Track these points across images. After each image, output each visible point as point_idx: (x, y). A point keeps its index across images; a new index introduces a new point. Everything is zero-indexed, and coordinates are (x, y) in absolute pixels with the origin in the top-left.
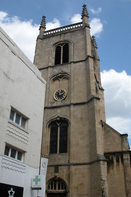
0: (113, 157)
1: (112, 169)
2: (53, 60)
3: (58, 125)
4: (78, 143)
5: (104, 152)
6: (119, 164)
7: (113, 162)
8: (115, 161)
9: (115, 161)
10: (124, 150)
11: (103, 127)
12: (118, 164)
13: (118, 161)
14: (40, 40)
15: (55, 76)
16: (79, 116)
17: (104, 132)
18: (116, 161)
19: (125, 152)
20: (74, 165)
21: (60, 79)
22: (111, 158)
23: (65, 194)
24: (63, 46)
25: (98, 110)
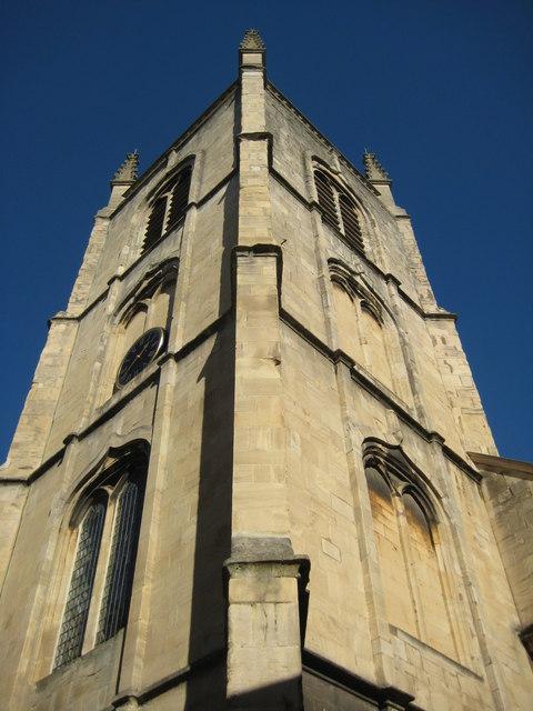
3: (110, 492)
14: (106, 223)
15: (131, 301)
21: (147, 301)
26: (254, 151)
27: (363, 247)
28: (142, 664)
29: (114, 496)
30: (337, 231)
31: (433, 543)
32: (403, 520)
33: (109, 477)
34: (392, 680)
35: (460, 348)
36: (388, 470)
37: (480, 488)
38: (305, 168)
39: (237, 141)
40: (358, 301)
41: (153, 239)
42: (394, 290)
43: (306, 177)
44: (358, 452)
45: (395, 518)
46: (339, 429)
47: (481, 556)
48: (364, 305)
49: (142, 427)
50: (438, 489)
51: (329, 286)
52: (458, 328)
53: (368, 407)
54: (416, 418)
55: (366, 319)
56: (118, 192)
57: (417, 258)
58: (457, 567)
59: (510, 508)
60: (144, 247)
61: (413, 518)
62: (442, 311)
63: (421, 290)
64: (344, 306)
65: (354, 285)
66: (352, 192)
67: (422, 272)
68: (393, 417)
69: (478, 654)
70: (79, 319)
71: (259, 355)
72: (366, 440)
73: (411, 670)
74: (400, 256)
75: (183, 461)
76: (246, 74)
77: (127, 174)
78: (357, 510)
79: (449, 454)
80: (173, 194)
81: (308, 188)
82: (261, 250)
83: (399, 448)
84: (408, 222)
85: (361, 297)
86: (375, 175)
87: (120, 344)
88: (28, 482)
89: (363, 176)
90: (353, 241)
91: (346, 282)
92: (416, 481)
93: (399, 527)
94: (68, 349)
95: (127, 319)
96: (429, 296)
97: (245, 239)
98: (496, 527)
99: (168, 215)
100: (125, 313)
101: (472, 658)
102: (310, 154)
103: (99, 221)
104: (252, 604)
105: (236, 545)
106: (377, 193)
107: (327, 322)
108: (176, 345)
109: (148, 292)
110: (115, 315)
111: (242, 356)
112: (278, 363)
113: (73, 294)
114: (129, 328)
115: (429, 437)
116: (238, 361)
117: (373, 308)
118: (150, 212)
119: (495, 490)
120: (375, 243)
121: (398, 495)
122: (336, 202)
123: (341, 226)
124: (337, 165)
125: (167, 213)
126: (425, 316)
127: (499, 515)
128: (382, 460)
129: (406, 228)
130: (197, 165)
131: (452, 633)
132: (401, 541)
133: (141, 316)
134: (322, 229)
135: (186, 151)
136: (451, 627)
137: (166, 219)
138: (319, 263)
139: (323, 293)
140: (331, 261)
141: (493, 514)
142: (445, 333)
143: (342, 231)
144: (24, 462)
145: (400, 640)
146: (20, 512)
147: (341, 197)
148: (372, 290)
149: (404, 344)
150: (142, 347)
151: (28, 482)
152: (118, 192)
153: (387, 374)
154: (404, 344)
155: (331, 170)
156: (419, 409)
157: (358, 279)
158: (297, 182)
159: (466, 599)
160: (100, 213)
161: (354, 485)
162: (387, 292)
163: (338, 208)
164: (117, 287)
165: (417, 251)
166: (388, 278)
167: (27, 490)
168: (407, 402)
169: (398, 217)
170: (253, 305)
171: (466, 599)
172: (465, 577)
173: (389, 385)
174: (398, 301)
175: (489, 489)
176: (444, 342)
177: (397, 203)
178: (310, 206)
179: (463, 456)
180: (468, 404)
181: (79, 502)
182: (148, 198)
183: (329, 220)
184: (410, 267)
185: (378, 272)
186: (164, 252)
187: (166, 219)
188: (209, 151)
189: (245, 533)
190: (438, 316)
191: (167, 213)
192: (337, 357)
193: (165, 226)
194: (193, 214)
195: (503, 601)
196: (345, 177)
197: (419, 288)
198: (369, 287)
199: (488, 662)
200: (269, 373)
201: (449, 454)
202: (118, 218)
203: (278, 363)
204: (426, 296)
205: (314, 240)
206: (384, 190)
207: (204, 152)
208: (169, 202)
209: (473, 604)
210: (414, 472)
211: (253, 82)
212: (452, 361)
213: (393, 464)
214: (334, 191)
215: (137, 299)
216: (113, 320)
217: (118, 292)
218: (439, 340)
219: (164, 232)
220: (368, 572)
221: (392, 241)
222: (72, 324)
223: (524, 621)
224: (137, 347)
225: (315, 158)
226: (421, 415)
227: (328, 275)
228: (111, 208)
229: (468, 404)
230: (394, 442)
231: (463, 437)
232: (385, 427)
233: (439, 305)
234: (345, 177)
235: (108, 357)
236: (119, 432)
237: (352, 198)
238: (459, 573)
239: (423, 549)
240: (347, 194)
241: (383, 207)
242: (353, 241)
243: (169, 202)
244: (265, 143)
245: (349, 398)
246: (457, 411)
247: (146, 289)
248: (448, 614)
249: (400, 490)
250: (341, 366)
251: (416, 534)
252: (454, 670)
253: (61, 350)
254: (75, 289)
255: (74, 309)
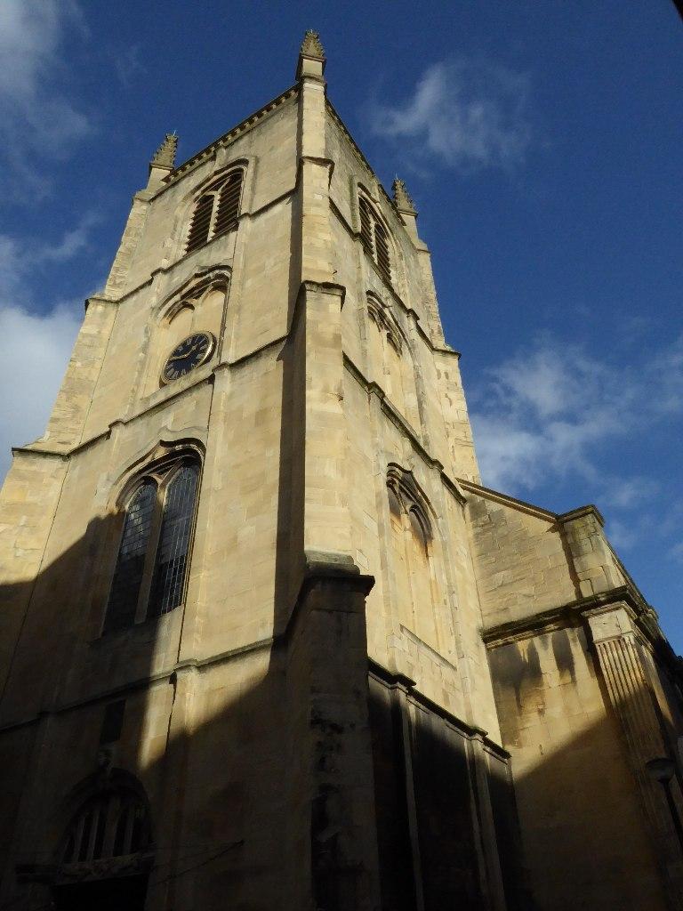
0: (537, 641)
1: (541, 712)
2: (179, 248)
3: (160, 481)
4: (235, 538)
5: (81, 320)
6: (574, 681)
7: (533, 671)
8: (547, 662)
9: (547, 662)
10: (587, 593)
11: (467, 508)
12: (568, 678)
13: (565, 663)
14: (145, 207)
15: (177, 297)
16: (251, 408)
17: (475, 527)
18: (553, 663)
19: (594, 604)
20: (202, 667)
21: (193, 302)
22: (524, 656)
23: (134, 888)
24: (220, 190)
25: (329, 337)
26: (316, 177)
27: (390, 278)
28: (199, 639)
29: (163, 486)
30: (373, 260)
31: (427, 556)
32: (409, 535)
33: (159, 466)
34: (401, 669)
35: (460, 385)
36: (402, 488)
37: (463, 510)
38: (352, 195)
39: (300, 163)
40: (385, 332)
41: (197, 241)
42: (413, 326)
43: (352, 204)
44: (383, 478)
45: (403, 532)
46: (371, 455)
47: (461, 569)
48: (389, 336)
49: (194, 427)
50: (435, 510)
51: (367, 320)
52: (460, 366)
53: (390, 433)
54: (422, 444)
55: (388, 348)
56: (158, 174)
57: (432, 294)
58: (444, 577)
59: (488, 530)
60: (189, 243)
61: (415, 533)
62: (448, 348)
63: (433, 325)
64: (376, 337)
65: (382, 316)
66: (387, 223)
67: (435, 308)
68: (408, 445)
69: (453, 649)
70: (117, 303)
71: (326, 390)
72: (390, 465)
73: (411, 660)
74: (418, 290)
75: (237, 466)
76: (307, 85)
77: (166, 154)
78: (381, 526)
79: (445, 479)
80: (222, 195)
81: (354, 220)
82: (328, 287)
83: (410, 472)
84: (427, 256)
85: (387, 329)
86: (403, 204)
87: (168, 339)
88: (66, 457)
89: (392, 202)
90: (383, 267)
91: (378, 315)
92: (419, 501)
93: (405, 540)
94: (106, 332)
95: (172, 314)
96: (439, 332)
97: (312, 271)
98: (473, 544)
99: (219, 213)
100: (170, 309)
101: (450, 652)
102: (356, 181)
103: (137, 203)
104: (330, 612)
105: (308, 555)
106: (404, 223)
107: (364, 352)
108: (230, 356)
109: (197, 292)
110: (160, 309)
111: (311, 388)
112: (341, 399)
113: (110, 276)
114: (172, 323)
115: (433, 463)
116: (308, 393)
117: (396, 341)
118: (194, 207)
119: (477, 512)
120: (400, 276)
121: (406, 513)
122: (372, 231)
123: (375, 256)
124: (376, 194)
125: (214, 215)
126: (433, 349)
127: (477, 535)
128: (397, 482)
129: (425, 260)
130: (248, 172)
131: (436, 630)
132: (406, 553)
133: (187, 313)
134: (363, 259)
135: (238, 152)
136: (436, 627)
137: (213, 221)
138: (360, 294)
139: (362, 326)
140: (369, 293)
141: (471, 534)
142: (449, 369)
143: (376, 261)
144: (64, 438)
145: (405, 636)
146: (60, 484)
147: (377, 226)
148: (396, 323)
149: (418, 376)
150: (190, 347)
151: (66, 457)
152: (158, 174)
153: (404, 403)
154: (418, 376)
155: (371, 198)
156: (426, 437)
157: (386, 311)
158: (345, 210)
159: (449, 604)
160: (138, 195)
161: (379, 504)
162: (408, 324)
163: (373, 238)
164: (161, 280)
165: (433, 287)
166: (410, 312)
167: (66, 464)
168: (417, 430)
169: (419, 250)
170: (319, 339)
171: (449, 604)
172: (450, 586)
173: (403, 414)
174: (414, 335)
175: (472, 513)
176: (447, 377)
177: (420, 237)
178: (354, 235)
179: (453, 480)
180: (461, 435)
181: (126, 486)
182: (193, 192)
183: (368, 250)
184: (426, 301)
185: (402, 305)
186: (210, 256)
187: (213, 221)
188: (267, 156)
189: (315, 548)
190: (445, 352)
191: (214, 215)
192: (373, 387)
193: (212, 228)
194: (246, 225)
195: (473, 607)
196: (381, 207)
197: (431, 323)
198: (394, 320)
199: (461, 656)
200: (334, 408)
201: (445, 479)
202: (160, 203)
203: (341, 399)
204: (436, 331)
205: (356, 271)
206: (409, 220)
207: (257, 161)
208: (216, 203)
209: (454, 609)
210: (419, 493)
211: (314, 93)
212: (452, 395)
213: (405, 486)
214: (371, 219)
215: (183, 297)
216: (156, 316)
217: (162, 285)
218: (443, 375)
219: (211, 234)
220: (387, 579)
221: (415, 275)
222: (111, 307)
223: (486, 625)
224: (185, 346)
225: (360, 185)
226: (426, 443)
227: (365, 305)
228: (149, 192)
229: (461, 435)
230: (408, 468)
231: (454, 464)
232: (402, 453)
233: (447, 342)
234: (381, 207)
235: (152, 349)
236: (173, 425)
237: (385, 228)
238: (446, 581)
239: (420, 558)
240: (382, 223)
241: (409, 239)
242: (383, 267)
243: (216, 203)
244: (327, 170)
245: (378, 427)
246: (451, 441)
247: (193, 289)
248: (434, 614)
249: (408, 508)
250: (374, 396)
251: (416, 547)
252: (437, 661)
253: (99, 332)
254: (112, 272)
255: (111, 292)
